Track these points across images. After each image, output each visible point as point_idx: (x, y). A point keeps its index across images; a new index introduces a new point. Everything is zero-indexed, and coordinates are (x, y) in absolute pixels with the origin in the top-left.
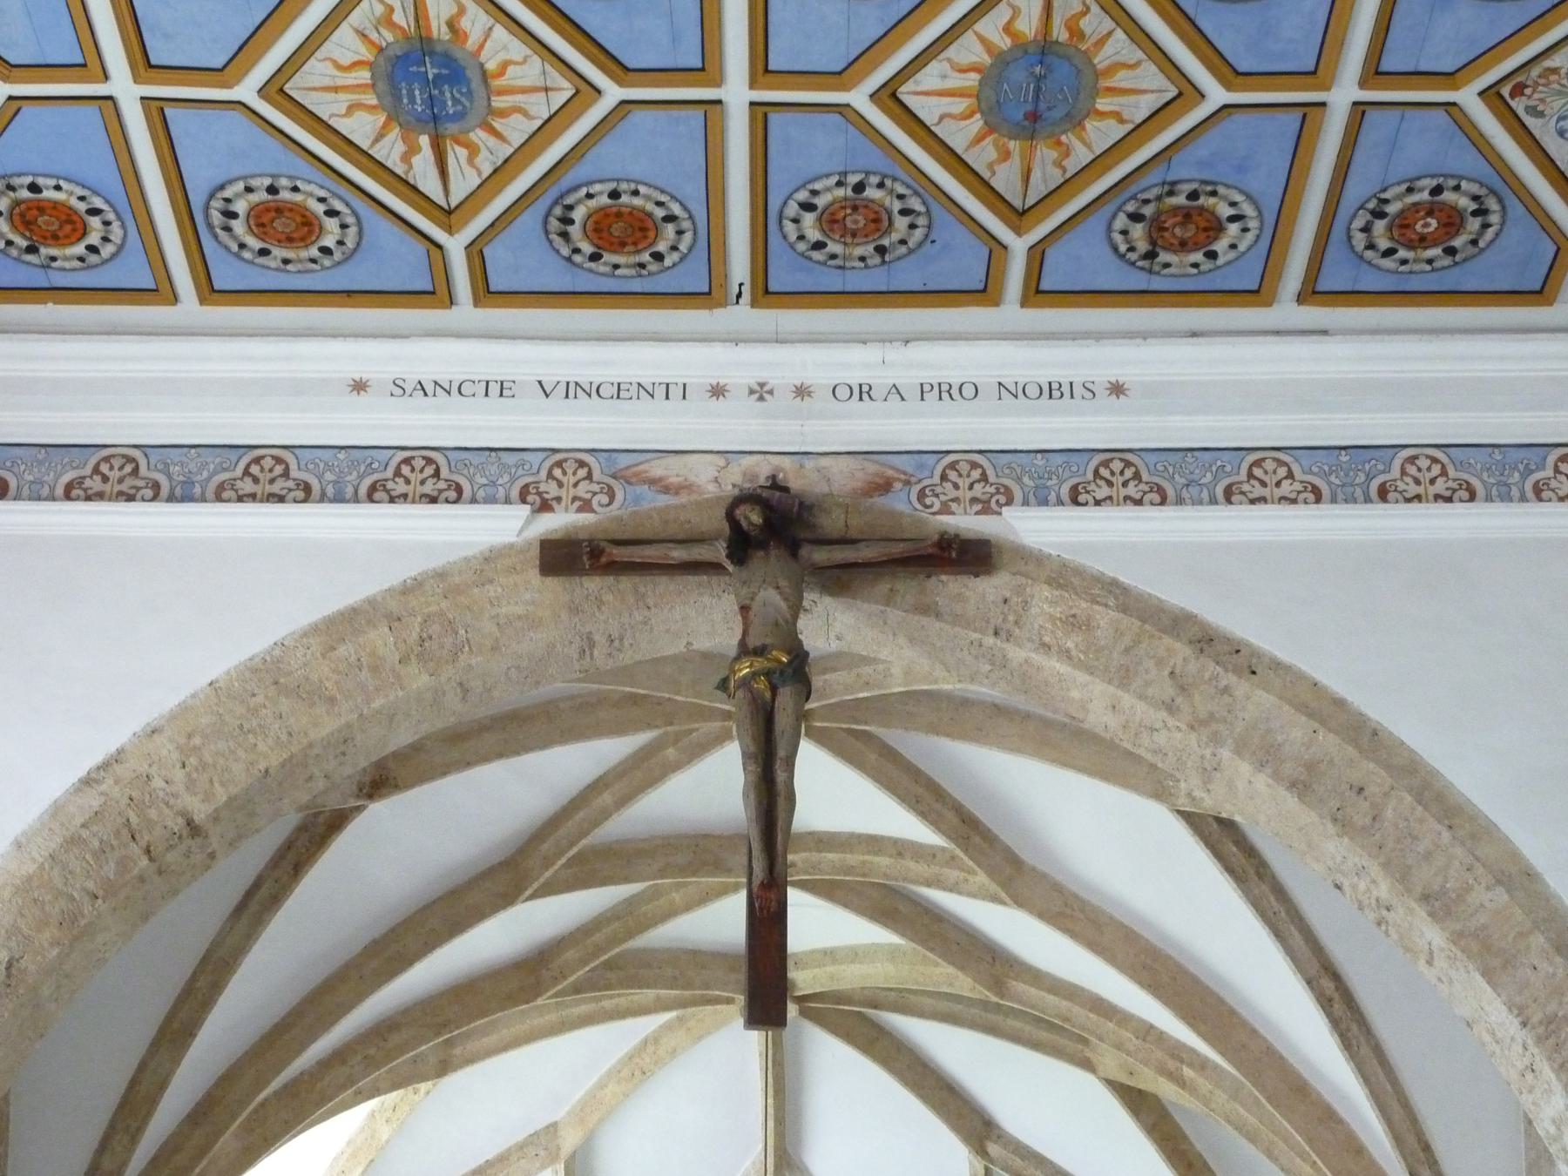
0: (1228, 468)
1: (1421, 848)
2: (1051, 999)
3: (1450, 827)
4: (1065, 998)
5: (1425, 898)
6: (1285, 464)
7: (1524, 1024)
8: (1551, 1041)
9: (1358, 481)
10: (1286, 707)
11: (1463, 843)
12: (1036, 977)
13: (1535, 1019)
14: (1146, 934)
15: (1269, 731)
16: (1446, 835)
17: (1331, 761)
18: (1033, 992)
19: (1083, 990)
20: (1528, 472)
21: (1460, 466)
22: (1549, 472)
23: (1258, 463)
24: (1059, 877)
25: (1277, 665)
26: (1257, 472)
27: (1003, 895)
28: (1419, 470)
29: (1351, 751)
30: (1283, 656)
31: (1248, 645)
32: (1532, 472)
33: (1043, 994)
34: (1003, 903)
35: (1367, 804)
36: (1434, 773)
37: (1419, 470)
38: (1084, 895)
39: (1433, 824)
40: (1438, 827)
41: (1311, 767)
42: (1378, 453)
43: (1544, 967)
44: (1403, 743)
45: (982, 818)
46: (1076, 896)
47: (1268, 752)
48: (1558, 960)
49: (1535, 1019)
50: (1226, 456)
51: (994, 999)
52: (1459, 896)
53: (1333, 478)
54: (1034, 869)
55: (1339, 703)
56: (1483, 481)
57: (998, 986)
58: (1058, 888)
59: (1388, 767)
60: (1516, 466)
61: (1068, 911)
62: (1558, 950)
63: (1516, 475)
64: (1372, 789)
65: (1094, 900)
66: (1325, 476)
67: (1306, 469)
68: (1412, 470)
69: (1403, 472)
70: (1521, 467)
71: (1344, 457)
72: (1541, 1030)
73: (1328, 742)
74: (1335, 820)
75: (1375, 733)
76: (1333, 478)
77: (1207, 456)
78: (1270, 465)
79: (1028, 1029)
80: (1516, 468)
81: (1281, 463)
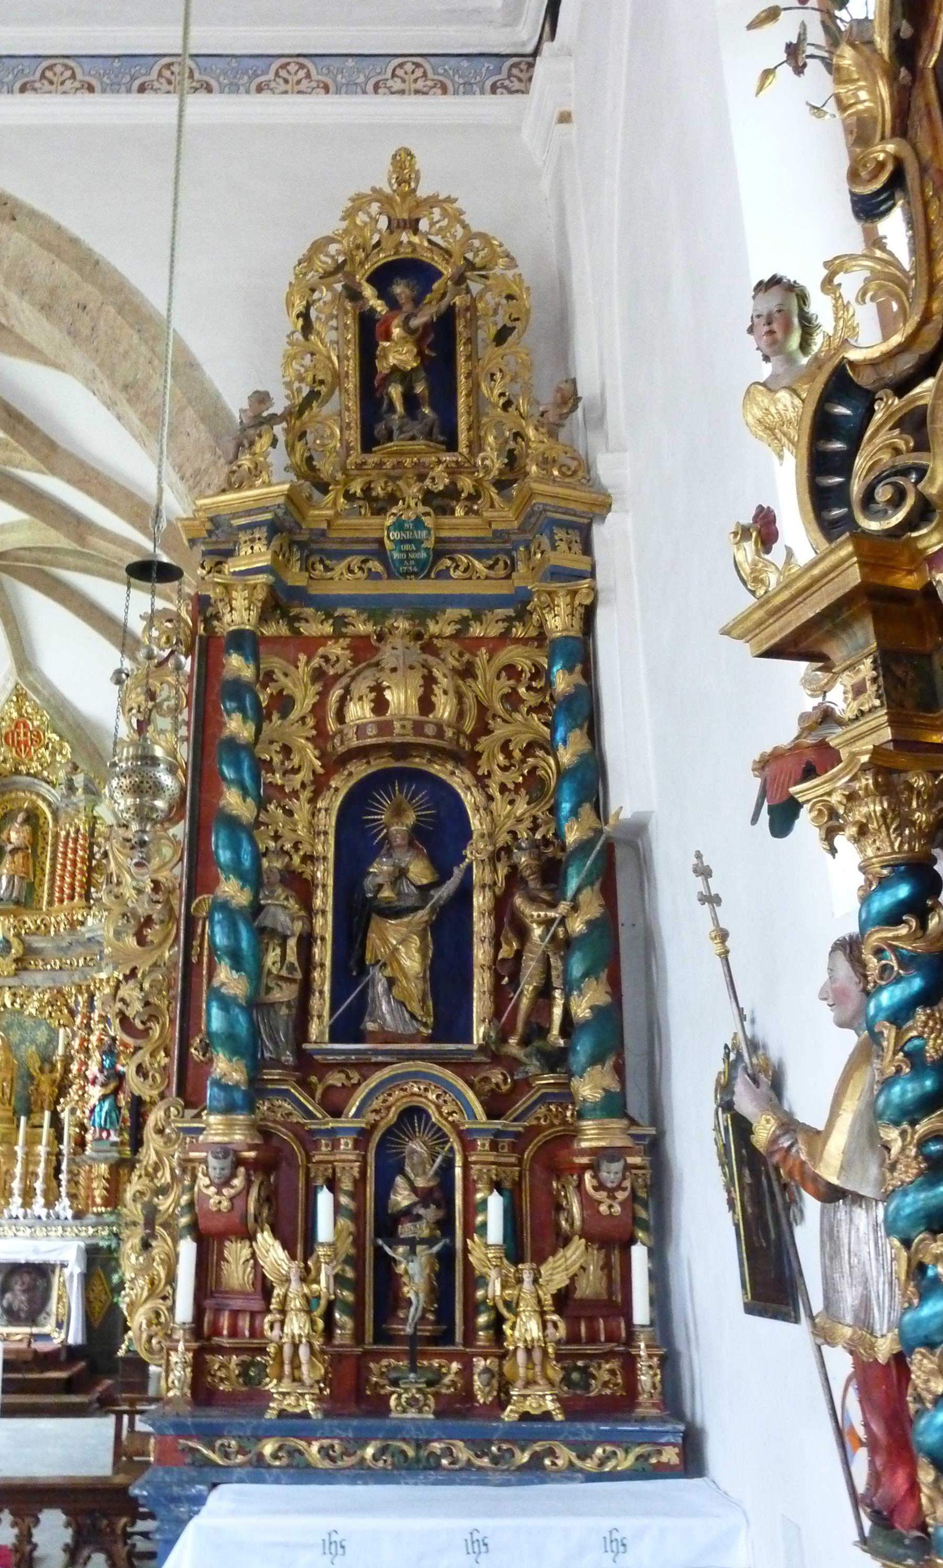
0: (27, 71)
1: (121, 350)
2: (112, 547)
3: (139, 331)
4: (120, 546)
5: (126, 387)
6: (71, 68)
7: (182, 478)
8: (196, 490)
9: (124, 81)
10: (34, 245)
11: (146, 343)
12: (104, 533)
13: (188, 475)
14: (140, 494)
15: (25, 265)
16: (136, 337)
17: (65, 287)
18: (102, 544)
19: (130, 541)
20: (256, 75)
21: (204, 70)
22: (271, 76)
23: (50, 68)
24: (82, 456)
25: (33, 214)
26: (49, 74)
27: (43, 468)
28: (172, 73)
29: (76, 276)
30: (39, 207)
31: (15, 200)
32: (258, 76)
33: (107, 544)
34: (43, 473)
35: (88, 318)
36: (135, 292)
37: (172, 73)
38: (100, 469)
39: (128, 330)
40: (131, 331)
41: (52, 292)
42: (142, 61)
43: (194, 434)
44: (116, 270)
45: (24, 413)
46: (93, 469)
47: (26, 283)
48: (202, 427)
49: (188, 475)
50: (26, 62)
51: (79, 548)
52: (145, 384)
53: (105, 79)
54: (65, 451)
55: (74, 241)
56: (219, 83)
57: (81, 540)
58: (81, 464)
59: (102, 288)
60: (247, 71)
61: (87, 478)
62: (202, 419)
63: (246, 78)
64: (91, 306)
65: (106, 472)
66: (100, 77)
67: (86, 71)
68: (167, 73)
69: (160, 75)
70: (250, 72)
71: (117, 63)
72: (191, 482)
73: (62, 268)
74: (69, 333)
75: (97, 263)
76: (105, 79)
77: (13, 62)
78: (58, 69)
79: (101, 566)
80: (246, 73)
81: (67, 67)
